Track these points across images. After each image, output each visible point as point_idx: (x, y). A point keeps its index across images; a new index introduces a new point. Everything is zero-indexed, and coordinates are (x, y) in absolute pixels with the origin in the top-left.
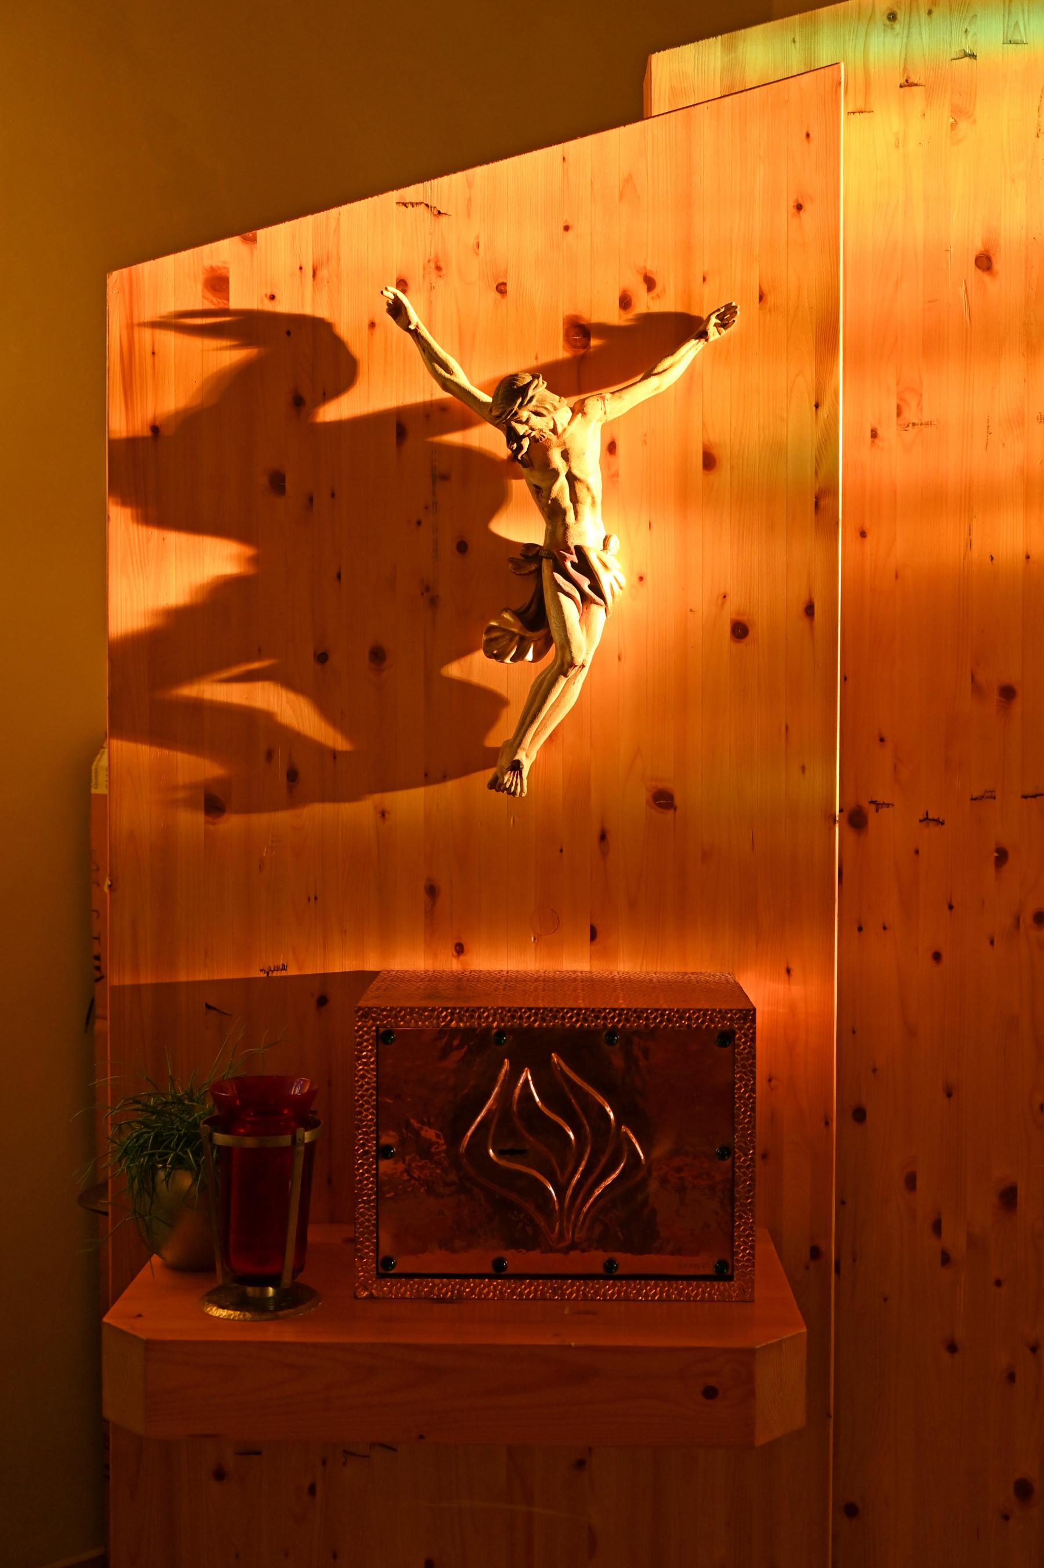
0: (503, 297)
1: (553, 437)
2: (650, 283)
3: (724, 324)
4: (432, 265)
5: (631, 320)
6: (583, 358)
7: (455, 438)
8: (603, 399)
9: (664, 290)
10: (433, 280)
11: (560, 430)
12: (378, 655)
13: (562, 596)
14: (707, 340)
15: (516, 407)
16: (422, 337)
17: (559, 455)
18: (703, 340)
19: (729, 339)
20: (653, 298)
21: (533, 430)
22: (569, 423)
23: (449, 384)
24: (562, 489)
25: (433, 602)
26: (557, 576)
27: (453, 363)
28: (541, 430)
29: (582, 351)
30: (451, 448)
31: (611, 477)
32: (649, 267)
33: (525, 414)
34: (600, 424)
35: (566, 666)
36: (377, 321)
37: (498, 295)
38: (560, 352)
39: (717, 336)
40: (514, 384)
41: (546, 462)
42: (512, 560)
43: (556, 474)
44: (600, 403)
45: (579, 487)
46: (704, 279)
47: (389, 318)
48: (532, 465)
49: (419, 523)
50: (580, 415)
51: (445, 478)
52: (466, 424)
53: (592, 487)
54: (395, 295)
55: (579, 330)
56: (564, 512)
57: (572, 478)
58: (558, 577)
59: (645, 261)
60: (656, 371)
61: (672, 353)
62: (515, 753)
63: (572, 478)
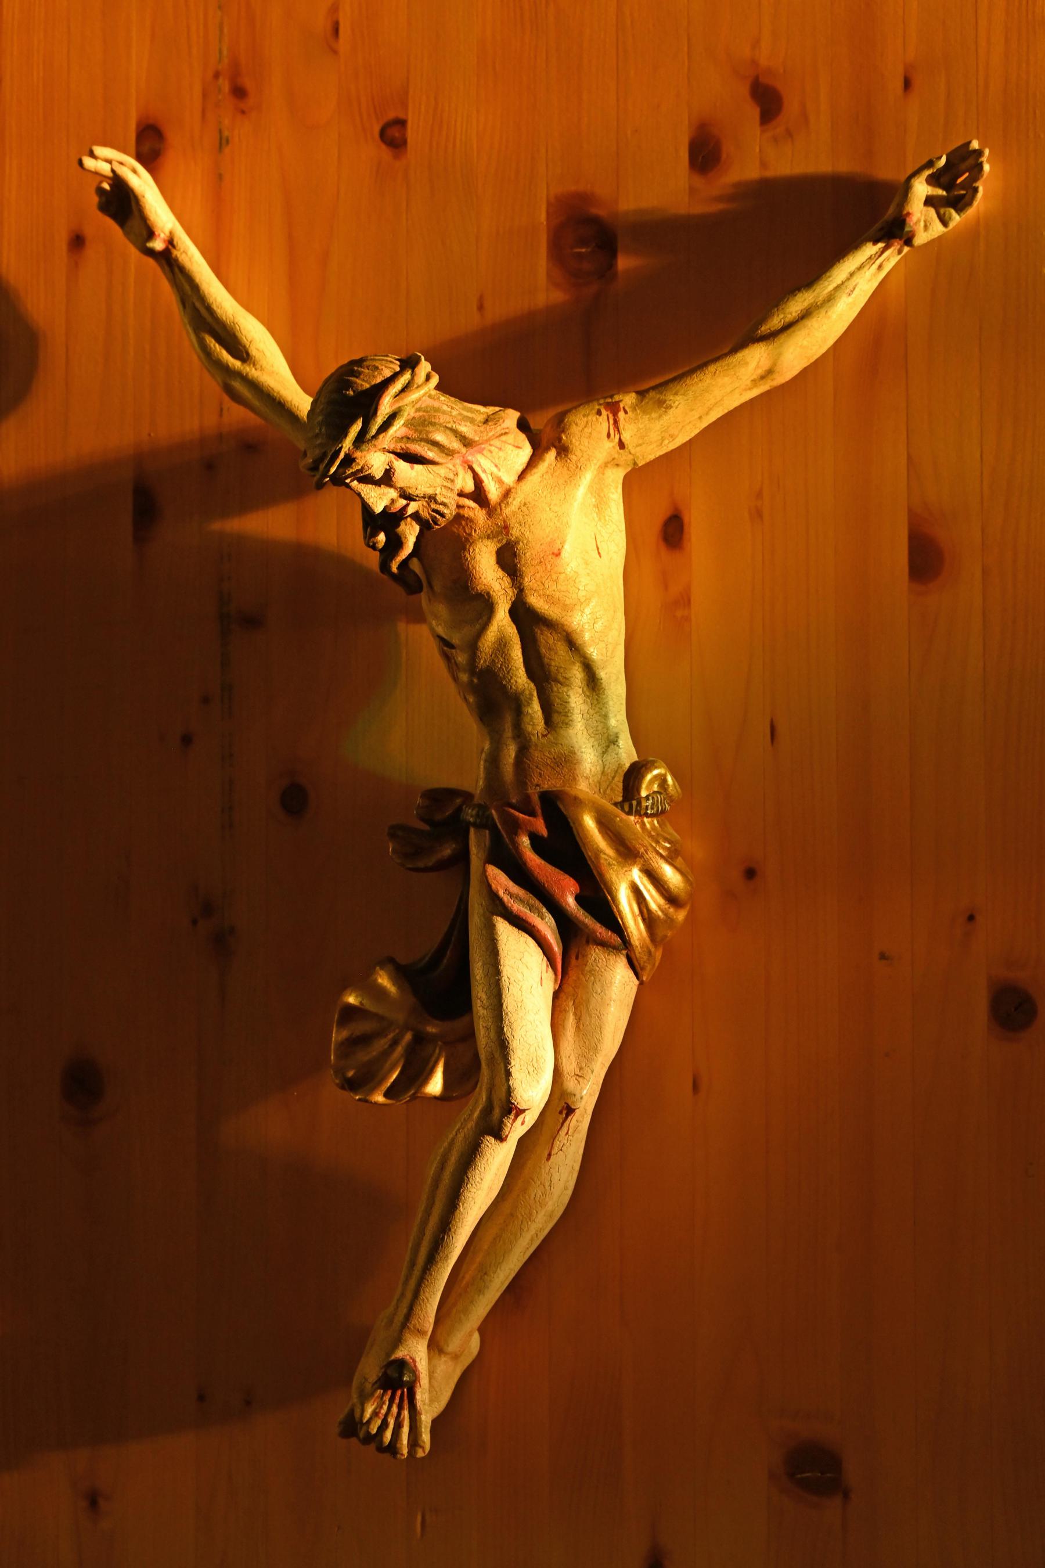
0: (397, 157)
1: (478, 514)
2: (767, 100)
3: (955, 186)
4: (225, 85)
5: (719, 199)
8: (614, 409)
10: (226, 122)
11: (493, 492)
12: (83, 1083)
13: (502, 927)
14: (908, 242)
15: (347, 444)
16: (182, 270)
17: (493, 560)
18: (896, 245)
19: (972, 235)
20: (775, 139)
22: (521, 477)
23: (237, 385)
24: (502, 645)
25: (222, 943)
26: (493, 871)
28: (432, 498)
32: (763, 62)
33: (376, 461)
34: (616, 477)
35: (497, 1112)
37: (385, 153)
38: (536, 286)
40: (349, 385)
42: (396, 832)
44: (602, 423)
45: (546, 639)
46: (907, 84)
49: (187, 740)
50: (552, 454)
51: (252, 622)
55: (586, 235)
56: (517, 704)
57: (525, 616)
58: (500, 881)
59: (756, 43)
60: (764, 329)
61: (811, 277)
62: (398, 1341)
63: (525, 616)
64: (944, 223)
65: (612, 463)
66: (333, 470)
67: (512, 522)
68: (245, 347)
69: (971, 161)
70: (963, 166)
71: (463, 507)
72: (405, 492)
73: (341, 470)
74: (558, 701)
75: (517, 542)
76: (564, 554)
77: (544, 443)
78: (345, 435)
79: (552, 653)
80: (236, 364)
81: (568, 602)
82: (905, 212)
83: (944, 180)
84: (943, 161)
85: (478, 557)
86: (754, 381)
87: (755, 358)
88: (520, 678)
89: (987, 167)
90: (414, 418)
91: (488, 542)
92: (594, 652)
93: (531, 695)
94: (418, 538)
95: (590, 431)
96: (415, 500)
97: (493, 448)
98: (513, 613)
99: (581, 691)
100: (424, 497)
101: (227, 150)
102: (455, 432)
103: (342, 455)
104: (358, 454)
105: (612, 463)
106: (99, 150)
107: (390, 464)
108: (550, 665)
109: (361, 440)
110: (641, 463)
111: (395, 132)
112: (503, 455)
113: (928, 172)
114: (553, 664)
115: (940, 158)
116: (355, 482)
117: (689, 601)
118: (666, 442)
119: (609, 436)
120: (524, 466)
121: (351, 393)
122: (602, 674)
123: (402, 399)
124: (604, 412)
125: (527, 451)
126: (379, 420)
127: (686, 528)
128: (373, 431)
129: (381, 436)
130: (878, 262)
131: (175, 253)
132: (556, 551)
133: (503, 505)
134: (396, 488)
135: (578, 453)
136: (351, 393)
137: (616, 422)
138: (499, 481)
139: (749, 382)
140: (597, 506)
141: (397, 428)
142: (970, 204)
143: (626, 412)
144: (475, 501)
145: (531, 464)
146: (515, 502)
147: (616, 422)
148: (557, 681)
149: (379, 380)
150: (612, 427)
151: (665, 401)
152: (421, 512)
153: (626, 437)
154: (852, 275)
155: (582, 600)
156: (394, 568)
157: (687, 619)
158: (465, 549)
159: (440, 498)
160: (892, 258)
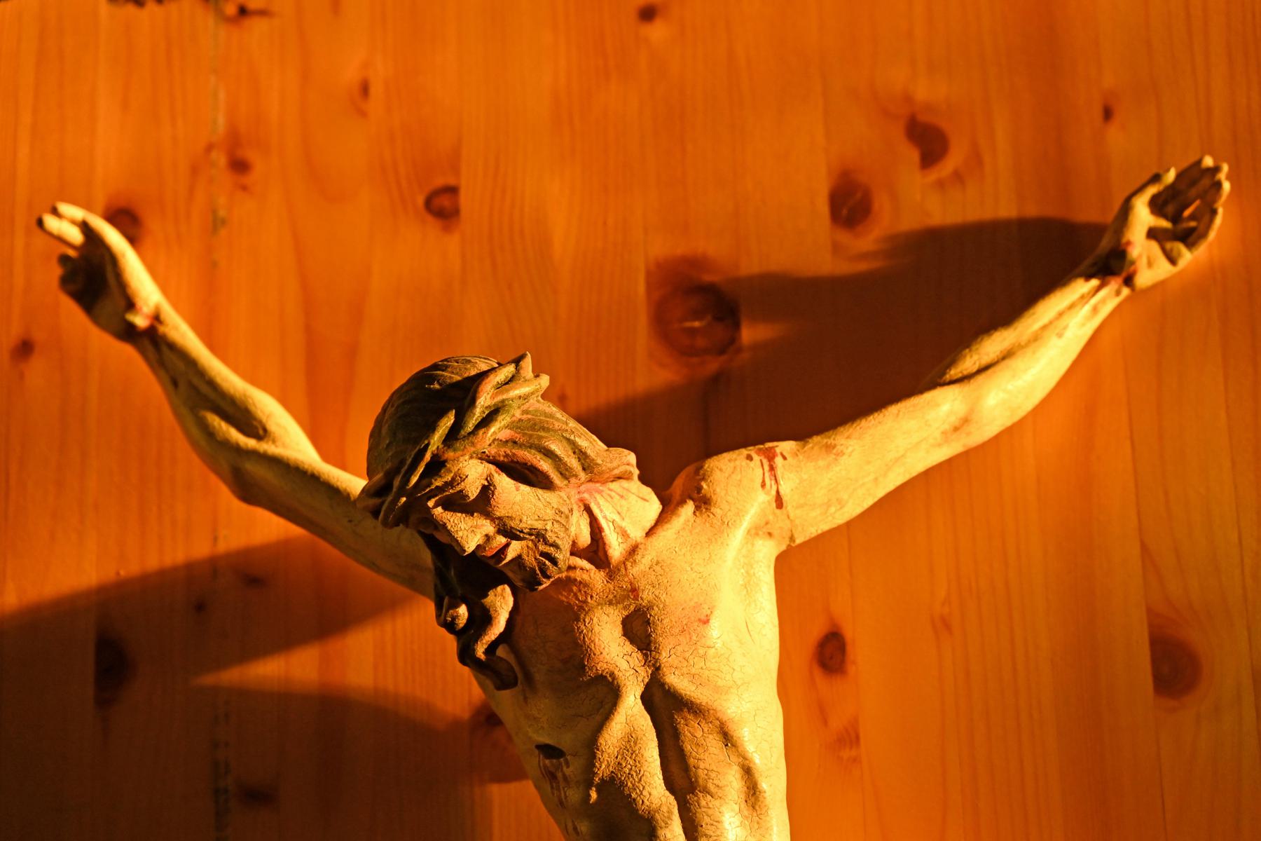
1: (596, 578)
2: (928, 142)
3: (1180, 228)
4: (220, 159)
6: (716, 380)
7: (296, 668)
9: (976, 159)
10: (222, 200)
11: (616, 549)
14: (1129, 281)
15: (436, 439)
16: (173, 347)
18: (1114, 284)
20: (940, 184)
21: (512, 534)
22: (650, 533)
24: (631, 743)
27: (267, 406)
29: (713, 365)
30: (284, 700)
31: (823, 741)
34: (767, 551)
36: (39, 336)
39: (1163, 269)
41: (575, 656)
43: (610, 691)
46: (1108, 114)
47: (71, 310)
48: (529, 678)
50: (689, 507)
51: (258, 796)
52: (330, 617)
53: (747, 736)
54: (85, 227)
57: (665, 705)
60: (954, 373)
63: (665, 705)
64: (1173, 261)
65: (762, 530)
66: (414, 479)
67: (642, 584)
68: (260, 422)
69: (1206, 182)
70: (1193, 192)
71: (575, 568)
72: (505, 525)
73: (425, 482)
74: (707, 820)
75: (650, 607)
76: (714, 622)
77: (677, 496)
78: (432, 428)
79: (701, 750)
80: (251, 443)
81: (720, 683)
82: (1124, 240)
83: (1170, 209)
84: (1171, 176)
85: (597, 629)
86: (944, 433)
87: (942, 405)
88: (654, 791)
89: (1227, 186)
90: (520, 420)
91: (610, 610)
92: (757, 760)
93: (670, 812)
94: (511, 613)
95: (737, 477)
96: (518, 538)
97: (613, 494)
98: (647, 700)
99: (736, 807)
100: (531, 535)
101: (223, 232)
102: (572, 444)
103: (428, 456)
104: (450, 454)
105: (762, 530)
106: (64, 208)
107: (489, 478)
108: (697, 768)
109: (452, 437)
110: (799, 540)
111: (445, 202)
112: (628, 508)
113: (1152, 190)
114: (702, 765)
115: (1168, 170)
116: (440, 509)
117: (858, 737)
118: (833, 509)
119: (763, 485)
120: (653, 523)
121: (437, 386)
122: (764, 785)
123: (508, 391)
124: (756, 458)
125: (655, 507)
126: (478, 413)
127: (849, 648)
128: (470, 426)
129: (481, 432)
130: (1094, 301)
131: (162, 329)
132: (703, 618)
133: (629, 564)
134: (493, 520)
135: (725, 506)
136: (437, 386)
137: (772, 468)
138: (624, 534)
139: (937, 434)
140: (745, 586)
141: (498, 429)
142: (1204, 235)
143: (785, 458)
144: (590, 561)
145: (661, 520)
146: (644, 561)
147: (772, 468)
148: (706, 791)
149: (473, 372)
150: (767, 475)
151: (834, 447)
152: (525, 557)
153: (785, 489)
154: (1061, 314)
155: (739, 683)
156: (480, 651)
157: (855, 760)
158: (578, 619)
159: (551, 537)
160: (1109, 298)
